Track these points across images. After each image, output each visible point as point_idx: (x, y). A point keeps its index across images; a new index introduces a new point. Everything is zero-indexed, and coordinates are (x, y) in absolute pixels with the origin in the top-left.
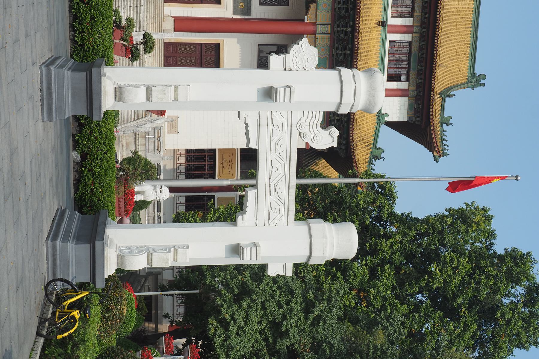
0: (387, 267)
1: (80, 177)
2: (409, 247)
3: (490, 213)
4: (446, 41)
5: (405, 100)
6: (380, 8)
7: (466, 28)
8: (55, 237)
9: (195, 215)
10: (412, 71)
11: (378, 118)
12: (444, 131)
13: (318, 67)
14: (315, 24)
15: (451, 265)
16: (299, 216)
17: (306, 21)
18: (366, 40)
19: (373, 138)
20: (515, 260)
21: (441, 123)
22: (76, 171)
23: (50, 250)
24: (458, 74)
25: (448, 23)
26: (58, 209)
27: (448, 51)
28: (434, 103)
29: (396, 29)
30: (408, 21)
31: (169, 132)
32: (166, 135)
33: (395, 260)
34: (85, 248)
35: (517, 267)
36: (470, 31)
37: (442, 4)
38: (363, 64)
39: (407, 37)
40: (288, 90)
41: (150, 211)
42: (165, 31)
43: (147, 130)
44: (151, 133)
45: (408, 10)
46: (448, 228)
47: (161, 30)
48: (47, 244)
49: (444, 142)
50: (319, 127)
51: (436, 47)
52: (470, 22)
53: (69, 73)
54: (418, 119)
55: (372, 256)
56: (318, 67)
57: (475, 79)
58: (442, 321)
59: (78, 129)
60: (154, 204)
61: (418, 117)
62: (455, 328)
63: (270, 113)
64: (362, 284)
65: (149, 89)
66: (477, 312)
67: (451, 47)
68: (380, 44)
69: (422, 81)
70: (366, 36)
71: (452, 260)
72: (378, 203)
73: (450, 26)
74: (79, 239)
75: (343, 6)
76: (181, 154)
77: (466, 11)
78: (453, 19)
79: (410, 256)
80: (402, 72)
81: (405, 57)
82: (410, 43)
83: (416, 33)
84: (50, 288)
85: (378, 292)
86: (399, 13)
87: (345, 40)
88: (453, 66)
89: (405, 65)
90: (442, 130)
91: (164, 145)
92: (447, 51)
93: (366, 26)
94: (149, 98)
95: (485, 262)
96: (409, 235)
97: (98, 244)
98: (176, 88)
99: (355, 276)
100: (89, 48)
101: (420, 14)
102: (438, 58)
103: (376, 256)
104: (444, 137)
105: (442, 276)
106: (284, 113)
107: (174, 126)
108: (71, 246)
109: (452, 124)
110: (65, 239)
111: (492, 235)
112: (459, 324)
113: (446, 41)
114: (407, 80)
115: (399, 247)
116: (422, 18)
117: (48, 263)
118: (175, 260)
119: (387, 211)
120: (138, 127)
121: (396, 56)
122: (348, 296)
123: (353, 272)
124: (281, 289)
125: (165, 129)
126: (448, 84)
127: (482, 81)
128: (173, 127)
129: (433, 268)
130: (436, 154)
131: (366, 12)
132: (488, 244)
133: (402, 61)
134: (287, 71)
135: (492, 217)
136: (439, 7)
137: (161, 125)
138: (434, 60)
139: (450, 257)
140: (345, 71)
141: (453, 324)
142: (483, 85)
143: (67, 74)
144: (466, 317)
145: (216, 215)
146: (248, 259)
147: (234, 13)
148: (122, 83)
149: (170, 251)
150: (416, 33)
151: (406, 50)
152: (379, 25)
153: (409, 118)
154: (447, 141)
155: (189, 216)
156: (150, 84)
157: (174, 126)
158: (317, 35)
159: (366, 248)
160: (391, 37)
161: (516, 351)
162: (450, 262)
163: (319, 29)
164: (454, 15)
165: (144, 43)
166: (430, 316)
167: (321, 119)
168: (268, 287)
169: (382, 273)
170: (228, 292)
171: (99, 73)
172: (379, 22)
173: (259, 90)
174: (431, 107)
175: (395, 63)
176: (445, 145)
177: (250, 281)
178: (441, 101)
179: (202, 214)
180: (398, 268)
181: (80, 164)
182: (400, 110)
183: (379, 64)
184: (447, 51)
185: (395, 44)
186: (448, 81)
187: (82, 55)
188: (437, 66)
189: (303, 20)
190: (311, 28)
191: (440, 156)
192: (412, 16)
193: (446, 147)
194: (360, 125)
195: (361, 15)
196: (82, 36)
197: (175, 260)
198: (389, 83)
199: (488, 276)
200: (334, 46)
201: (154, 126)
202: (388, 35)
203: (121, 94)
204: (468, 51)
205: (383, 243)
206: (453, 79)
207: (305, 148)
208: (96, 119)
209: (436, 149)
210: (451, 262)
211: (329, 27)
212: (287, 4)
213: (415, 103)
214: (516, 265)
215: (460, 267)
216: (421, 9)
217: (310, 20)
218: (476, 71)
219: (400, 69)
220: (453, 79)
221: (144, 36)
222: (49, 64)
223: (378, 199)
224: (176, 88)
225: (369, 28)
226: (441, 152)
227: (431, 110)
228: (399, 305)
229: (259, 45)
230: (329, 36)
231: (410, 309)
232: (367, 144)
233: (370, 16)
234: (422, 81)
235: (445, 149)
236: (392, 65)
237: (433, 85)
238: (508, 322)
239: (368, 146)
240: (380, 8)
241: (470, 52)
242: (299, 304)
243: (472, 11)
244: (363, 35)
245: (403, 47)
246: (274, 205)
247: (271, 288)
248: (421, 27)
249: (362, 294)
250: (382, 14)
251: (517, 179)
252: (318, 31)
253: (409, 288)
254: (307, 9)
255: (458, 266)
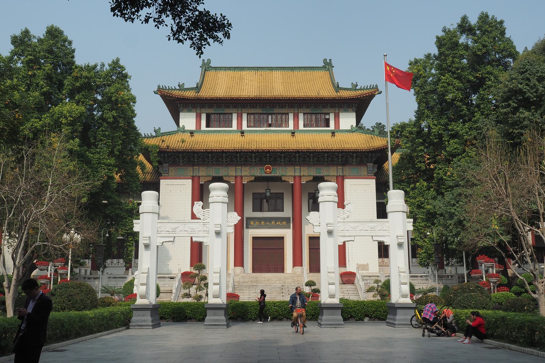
0: (450, 127)
1: (377, 318)
2: (436, 113)
3: (413, 60)
4: (303, 90)
5: (341, 115)
6: (283, 135)
7: (294, 75)
8: (394, 324)
9: (420, 253)
10: (323, 112)
11: (354, 132)
12: (361, 88)
13: (318, 211)
14: (295, 177)
15: (446, 87)
16: (418, 185)
17: (293, 183)
18: (304, 144)
19: (367, 135)
20: (442, 45)
21: (356, 90)
22: (374, 320)
23: (399, 326)
24: (324, 78)
25: (291, 90)
26: (386, 325)
27: (309, 87)
28: (342, 96)
29: (296, 124)
30: (291, 116)
31: (367, 270)
32: (369, 272)
33: (445, 122)
34: (399, 311)
35: (446, 44)
36: (296, 72)
37: (280, 96)
38: (319, 145)
39: (301, 116)
40: (328, 225)
41: (417, 282)
42: (303, 273)
43: (363, 284)
44: (366, 282)
45: (284, 117)
46: (422, 90)
47: (302, 275)
48: (397, 327)
49: (369, 87)
50: (344, 210)
51: (306, 98)
52: (290, 73)
53: (324, 316)
54: (354, 106)
55: (443, 137)
56: (318, 211)
57: (327, 66)
58: (485, 89)
59: (353, 318)
60: (412, 280)
61: (352, 105)
62: (490, 80)
63: (339, 232)
64: (462, 143)
65: (330, 284)
66: (479, 65)
67: (306, 85)
68: (306, 133)
69: (329, 105)
70: (301, 144)
71: (443, 87)
72: (408, 134)
73: (293, 87)
74: (395, 314)
75: (283, 160)
76: (383, 262)
77: (283, 76)
78: (288, 85)
79: (442, 112)
80: (323, 118)
81: (314, 117)
82: (304, 114)
83: (298, 110)
84: (414, 326)
85: (467, 133)
86: (286, 122)
87: (304, 157)
88: (318, 82)
89: (319, 116)
90: (361, 89)
91: (376, 273)
92: (309, 89)
93: (295, 144)
94: (333, 284)
95: (444, 65)
96: (427, 114)
97: (396, 306)
98: (328, 272)
99: (455, 149)
100: (314, 312)
101: (286, 109)
102: (313, 96)
103: (443, 135)
104: (365, 88)
105: (454, 92)
106: (339, 225)
107: (363, 266)
108: (398, 317)
109: (357, 82)
110: (395, 320)
111: (428, 56)
112: (487, 77)
113: (303, 90)
114: (329, 114)
115: (436, 120)
116: (289, 108)
117: (405, 327)
118: (405, 272)
119: (413, 128)
120: (362, 290)
121: (313, 123)
122: (470, 153)
123: (453, 150)
124: (458, 201)
125: (365, 273)
126: (330, 85)
127: (328, 61)
128: (365, 267)
129: (450, 96)
130: (376, 93)
131: (286, 145)
132: (434, 58)
133: (316, 118)
134: (321, 225)
135: (415, 59)
136: (282, 98)
137: (360, 276)
138: (315, 98)
139: (441, 88)
140: (320, 200)
141: (487, 82)
142: (330, 60)
143: (324, 317)
144: (482, 73)
145: (419, 239)
146: (404, 240)
147: (290, 228)
148: (328, 295)
149: (400, 275)
150: (298, 110)
151: (309, 116)
152: (294, 135)
153: (353, 111)
154: (367, 86)
155: (420, 257)
156: (328, 283)
157: (363, 266)
158: (302, 175)
159: (437, 141)
160: (301, 127)
161: (507, 36)
162: (444, 88)
163: (297, 174)
164: (286, 85)
165: (310, 286)
166: (482, 97)
167: (341, 209)
168: (457, 209)
169: (454, 131)
170: (460, 235)
171: (323, 304)
172: (292, 135)
173: (329, 237)
174: (345, 98)
175: (317, 122)
176: (370, 87)
177: (453, 220)
178: (341, 90)
179: (419, 249)
180: (451, 120)
181: (371, 318)
182: (348, 118)
183: (319, 134)
184: (309, 89)
185: (305, 123)
186: (328, 85)
187: (317, 315)
188: (318, 96)
189: (292, 184)
190: (297, 179)
191: (378, 90)
192: (288, 114)
193: (372, 86)
194: (358, 144)
195: (288, 148)
196: (308, 315)
197: (405, 272)
198: (330, 126)
199: (453, 62)
200: (308, 164)
201: (361, 280)
202: (202, 129)
203: (332, 295)
204: (308, 72)
205: (433, 131)
206: (327, 82)
207: (375, 180)
208: (342, 306)
209: (373, 93)
210: (444, 87)
211: (296, 167)
212: (283, 193)
213: (343, 108)
214: (445, 45)
215: (447, 81)
216: (283, 109)
217: (292, 180)
218: (321, 66)
219: (322, 119)
220: (327, 82)
221: (307, 286)
222: (320, 325)
223: (405, 135)
224: (328, 272)
225: (296, 142)
226: (375, 90)
227: (347, 98)
228: (475, 119)
229: (309, 211)
230: (302, 167)
231: (478, 111)
232: (371, 139)
233: (289, 142)
234: (329, 105)
235: (373, 87)
236: (319, 124)
237: (331, 98)
238: (484, 46)
239: (372, 138)
240: (283, 135)
241: (309, 71)
242: (467, 190)
243: (283, 72)
244: (300, 147)
245: (308, 118)
246: (379, 228)
247: (458, 207)
248: (294, 108)
249: (468, 143)
250: (287, 133)
251: (386, 56)
252: (299, 174)
253: (464, 112)
254: (284, 181)
255: (447, 83)
